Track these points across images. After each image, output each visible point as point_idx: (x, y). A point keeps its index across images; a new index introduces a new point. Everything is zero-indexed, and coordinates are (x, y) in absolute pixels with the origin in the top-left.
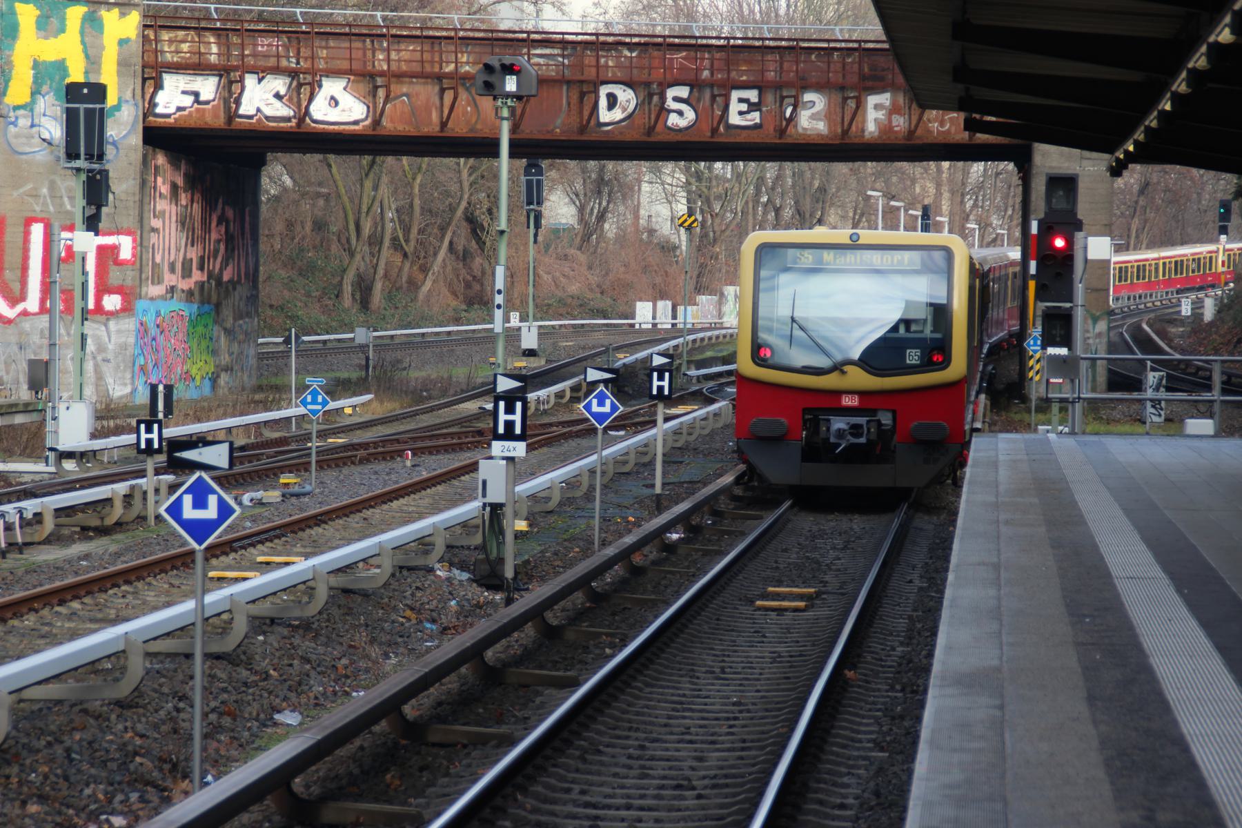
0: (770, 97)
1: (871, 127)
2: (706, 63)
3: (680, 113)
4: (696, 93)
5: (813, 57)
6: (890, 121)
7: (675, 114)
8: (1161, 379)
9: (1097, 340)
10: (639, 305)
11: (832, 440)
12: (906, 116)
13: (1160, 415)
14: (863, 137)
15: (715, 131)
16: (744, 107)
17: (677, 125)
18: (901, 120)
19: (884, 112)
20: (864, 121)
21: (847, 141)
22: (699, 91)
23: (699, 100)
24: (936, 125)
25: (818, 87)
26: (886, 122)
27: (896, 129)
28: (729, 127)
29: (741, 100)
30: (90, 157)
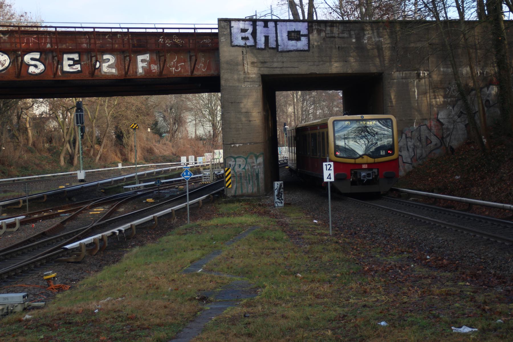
0: (85, 57)
1: (140, 70)
2: (48, 40)
3: (36, 66)
4: (43, 56)
5: (107, 37)
6: (150, 67)
7: (33, 67)
8: (281, 185)
9: (259, 167)
10: (182, 158)
11: (362, 178)
12: (158, 65)
13: (282, 203)
14: (137, 75)
15: (55, 74)
16: (71, 62)
17: (34, 72)
18: (156, 67)
19: (146, 63)
20: (136, 67)
21: (128, 78)
22: (46, 55)
23: (46, 59)
24: (174, 69)
25: (111, 51)
26: (148, 68)
27: (153, 71)
28: (64, 72)
29: (69, 59)
30: (80, 123)
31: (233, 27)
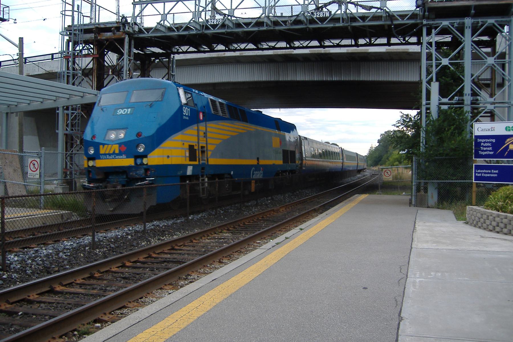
31: (282, 14)
